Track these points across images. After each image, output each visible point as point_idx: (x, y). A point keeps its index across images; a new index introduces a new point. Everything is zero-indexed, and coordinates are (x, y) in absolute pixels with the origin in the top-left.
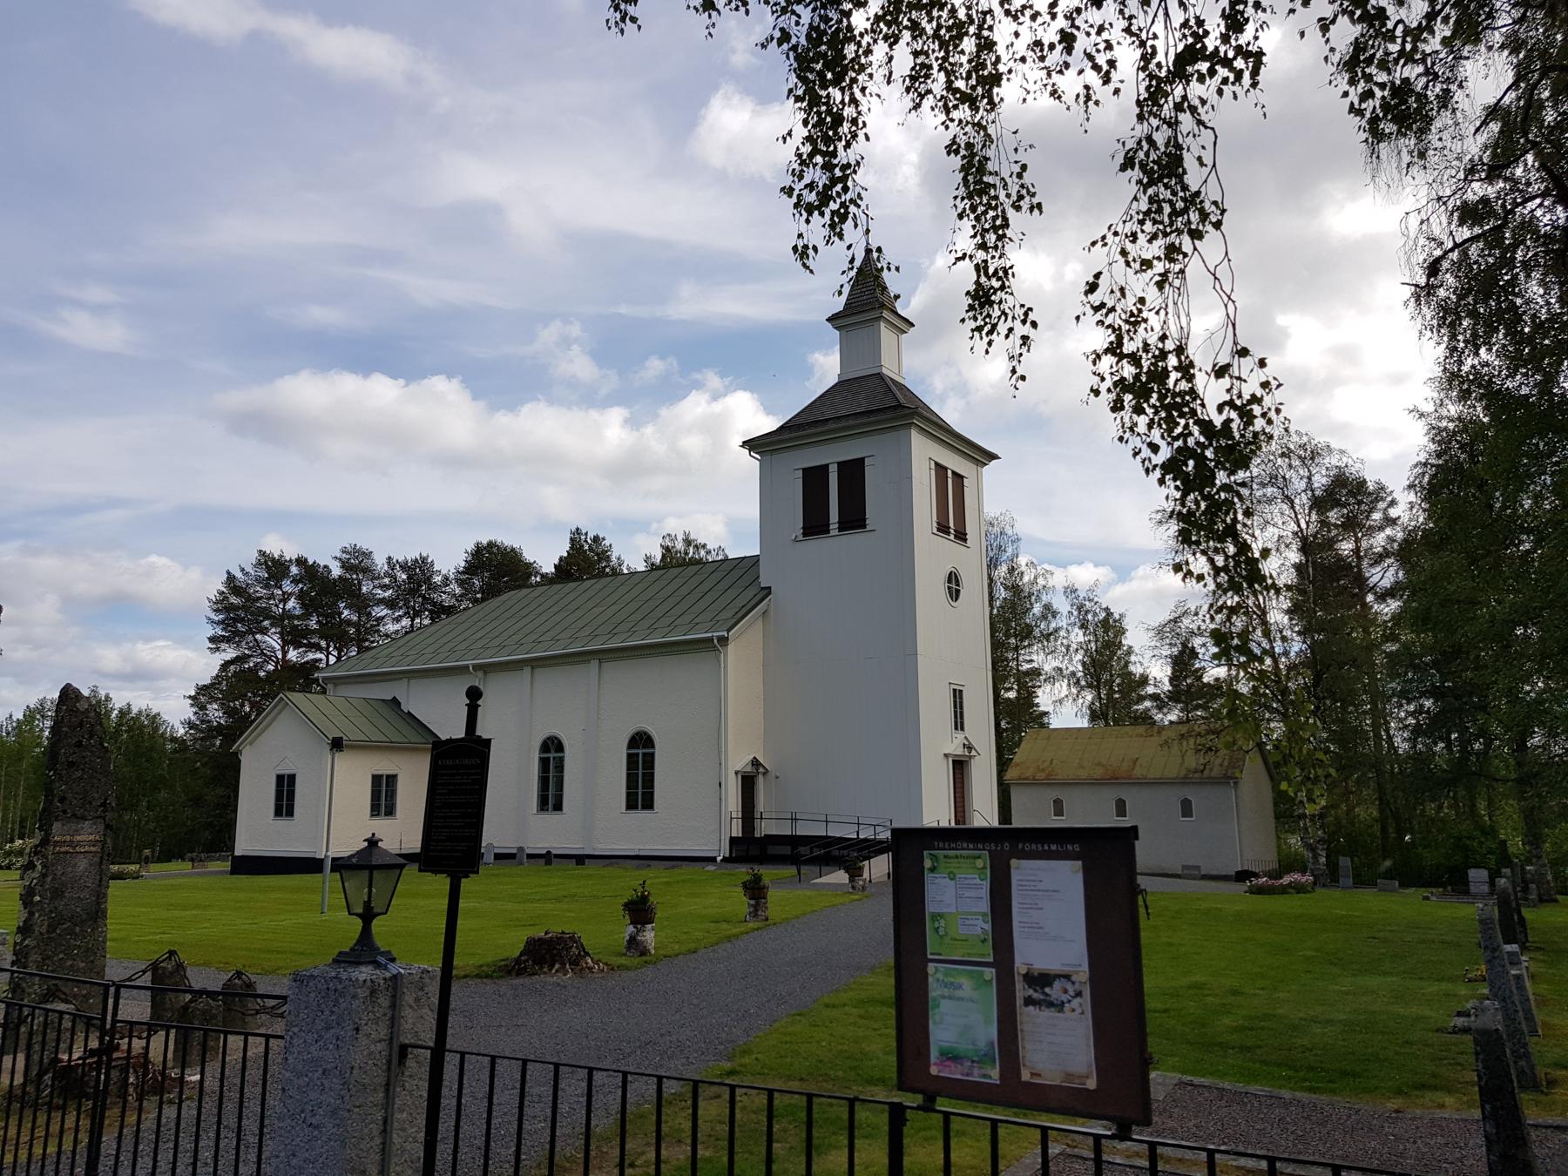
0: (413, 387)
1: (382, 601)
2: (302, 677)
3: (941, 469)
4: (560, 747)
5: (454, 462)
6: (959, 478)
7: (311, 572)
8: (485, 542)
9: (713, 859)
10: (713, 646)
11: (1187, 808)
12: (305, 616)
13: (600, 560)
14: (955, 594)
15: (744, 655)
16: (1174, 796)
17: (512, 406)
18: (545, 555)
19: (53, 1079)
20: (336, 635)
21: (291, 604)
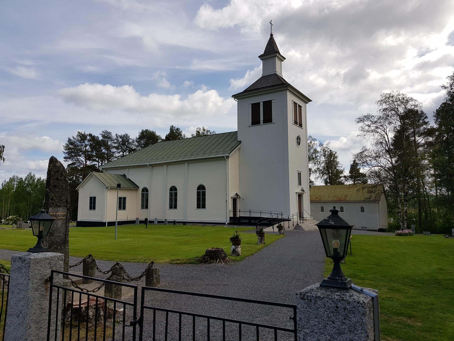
0: (118, 88)
1: (114, 147)
2: (93, 168)
3: (295, 104)
4: (176, 189)
5: (131, 111)
6: (300, 107)
7: (93, 138)
8: (144, 130)
9: (225, 224)
10: (224, 159)
11: (362, 210)
12: (92, 151)
13: (179, 135)
14: (299, 143)
15: (233, 162)
16: (359, 206)
17: (147, 95)
18: (163, 134)
19: (72, 314)
20: (101, 157)
21: (88, 147)
